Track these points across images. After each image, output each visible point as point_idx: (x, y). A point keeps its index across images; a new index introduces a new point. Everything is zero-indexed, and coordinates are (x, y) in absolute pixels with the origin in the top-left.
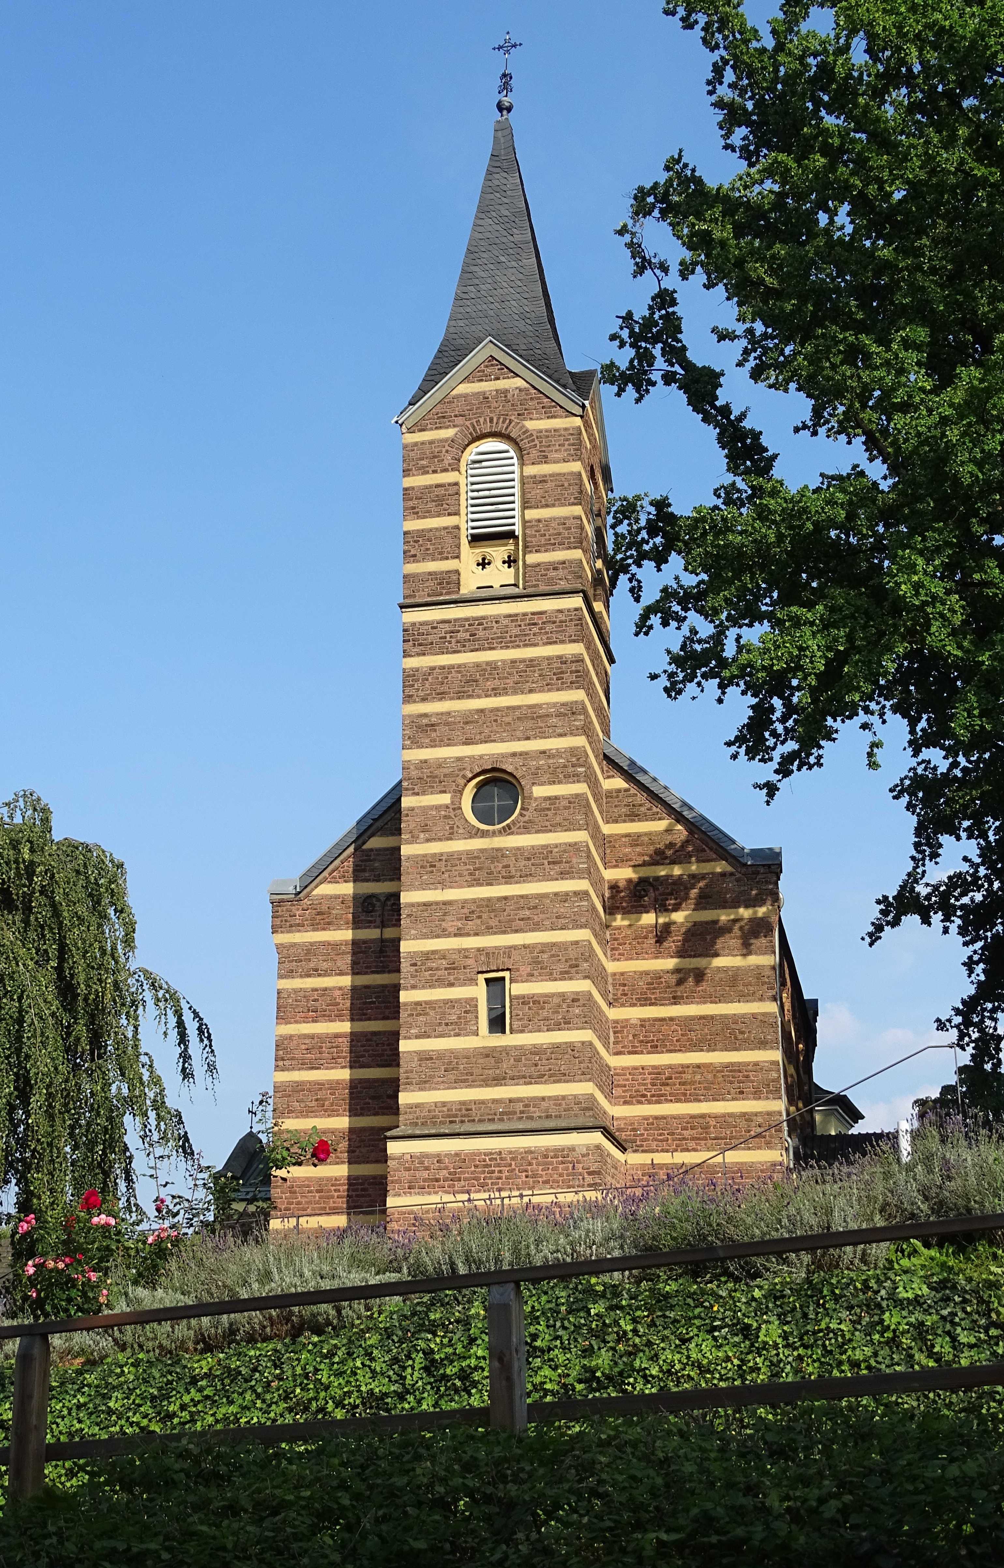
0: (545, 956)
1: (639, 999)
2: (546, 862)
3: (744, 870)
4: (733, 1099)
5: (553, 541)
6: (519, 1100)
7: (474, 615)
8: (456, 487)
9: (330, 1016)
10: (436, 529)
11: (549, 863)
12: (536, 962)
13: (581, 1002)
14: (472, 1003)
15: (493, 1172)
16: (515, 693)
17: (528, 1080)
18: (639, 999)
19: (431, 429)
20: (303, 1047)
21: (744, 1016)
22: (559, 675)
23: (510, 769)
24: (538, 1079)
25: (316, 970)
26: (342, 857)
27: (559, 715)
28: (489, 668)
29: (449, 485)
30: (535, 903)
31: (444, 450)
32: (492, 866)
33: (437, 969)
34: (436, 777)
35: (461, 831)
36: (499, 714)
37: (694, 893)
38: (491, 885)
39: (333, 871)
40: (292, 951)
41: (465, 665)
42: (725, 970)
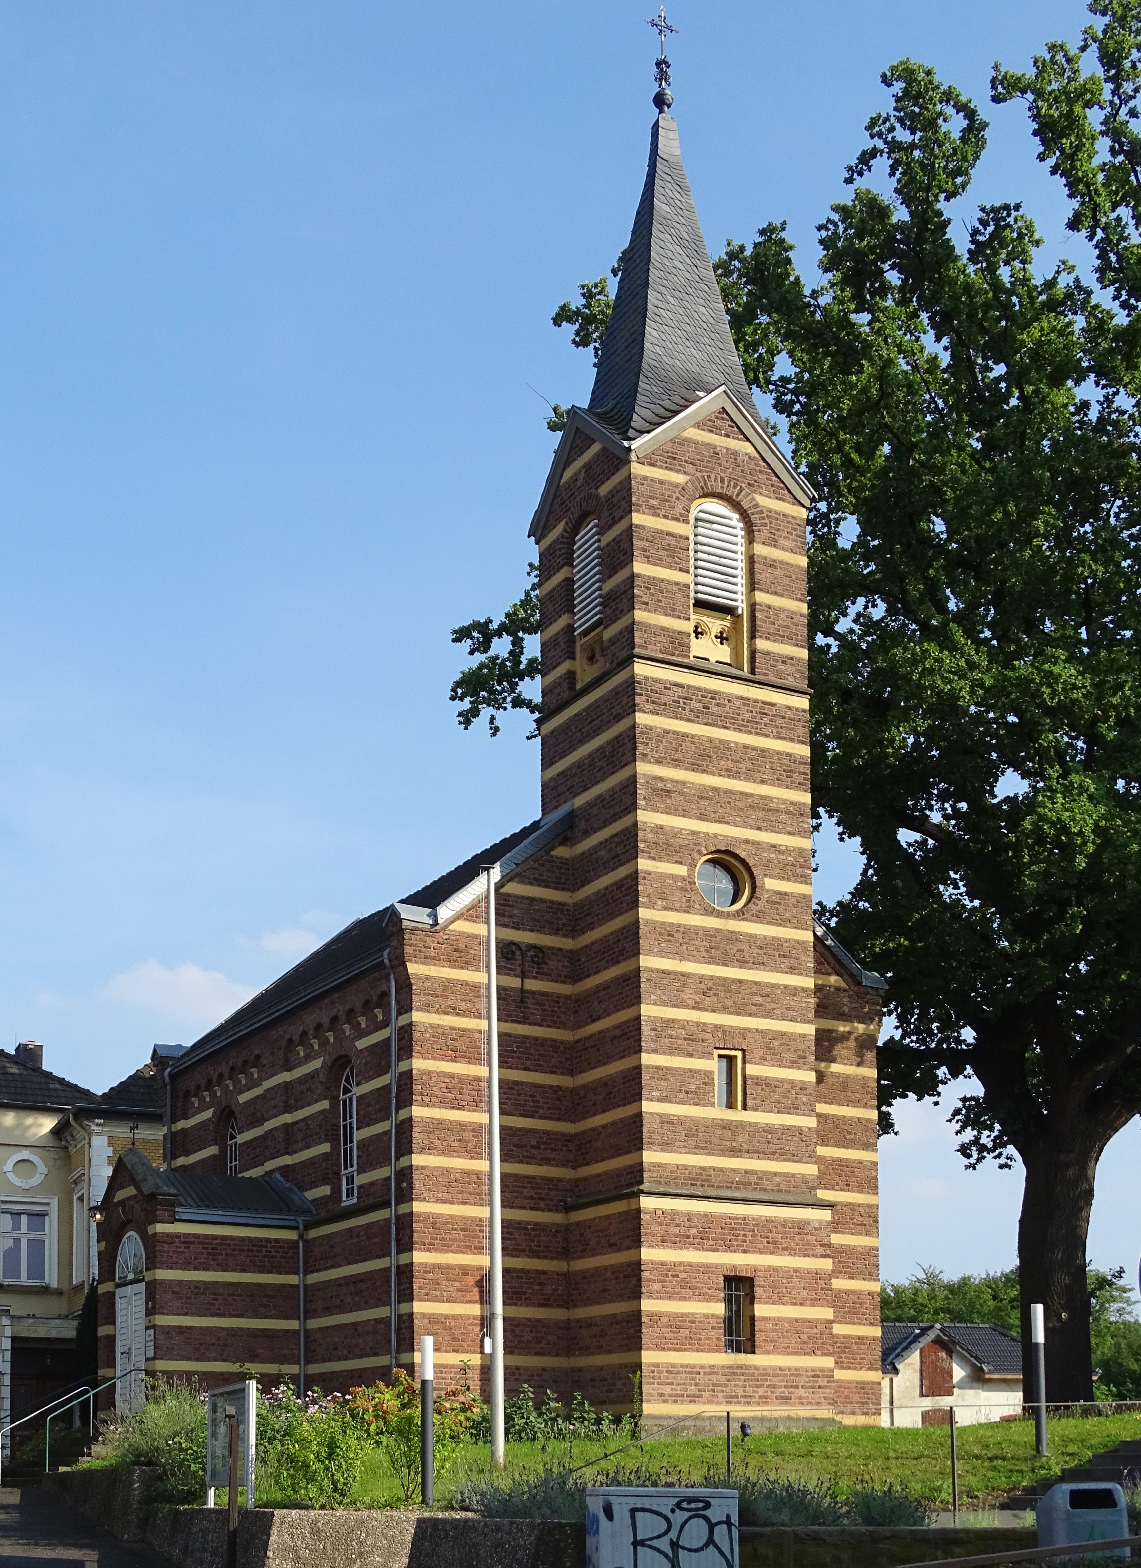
0: (776, 1043)
2: (777, 954)
3: (856, 989)
4: (841, 1190)
5: (781, 633)
6: (754, 1172)
9: (470, 1058)
12: (768, 1047)
14: (709, 1074)
15: (738, 1235)
16: (747, 779)
17: (761, 1156)
19: (661, 467)
20: (444, 1085)
21: (851, 1119)
23: (743, 855)
24: (771, 1155)
25: (454, 1009)
29: (681, 537)
30: (767, 991)
31: (675, 496)
32: (728, 947)
33: (676, 1038)
40: (428, 984)
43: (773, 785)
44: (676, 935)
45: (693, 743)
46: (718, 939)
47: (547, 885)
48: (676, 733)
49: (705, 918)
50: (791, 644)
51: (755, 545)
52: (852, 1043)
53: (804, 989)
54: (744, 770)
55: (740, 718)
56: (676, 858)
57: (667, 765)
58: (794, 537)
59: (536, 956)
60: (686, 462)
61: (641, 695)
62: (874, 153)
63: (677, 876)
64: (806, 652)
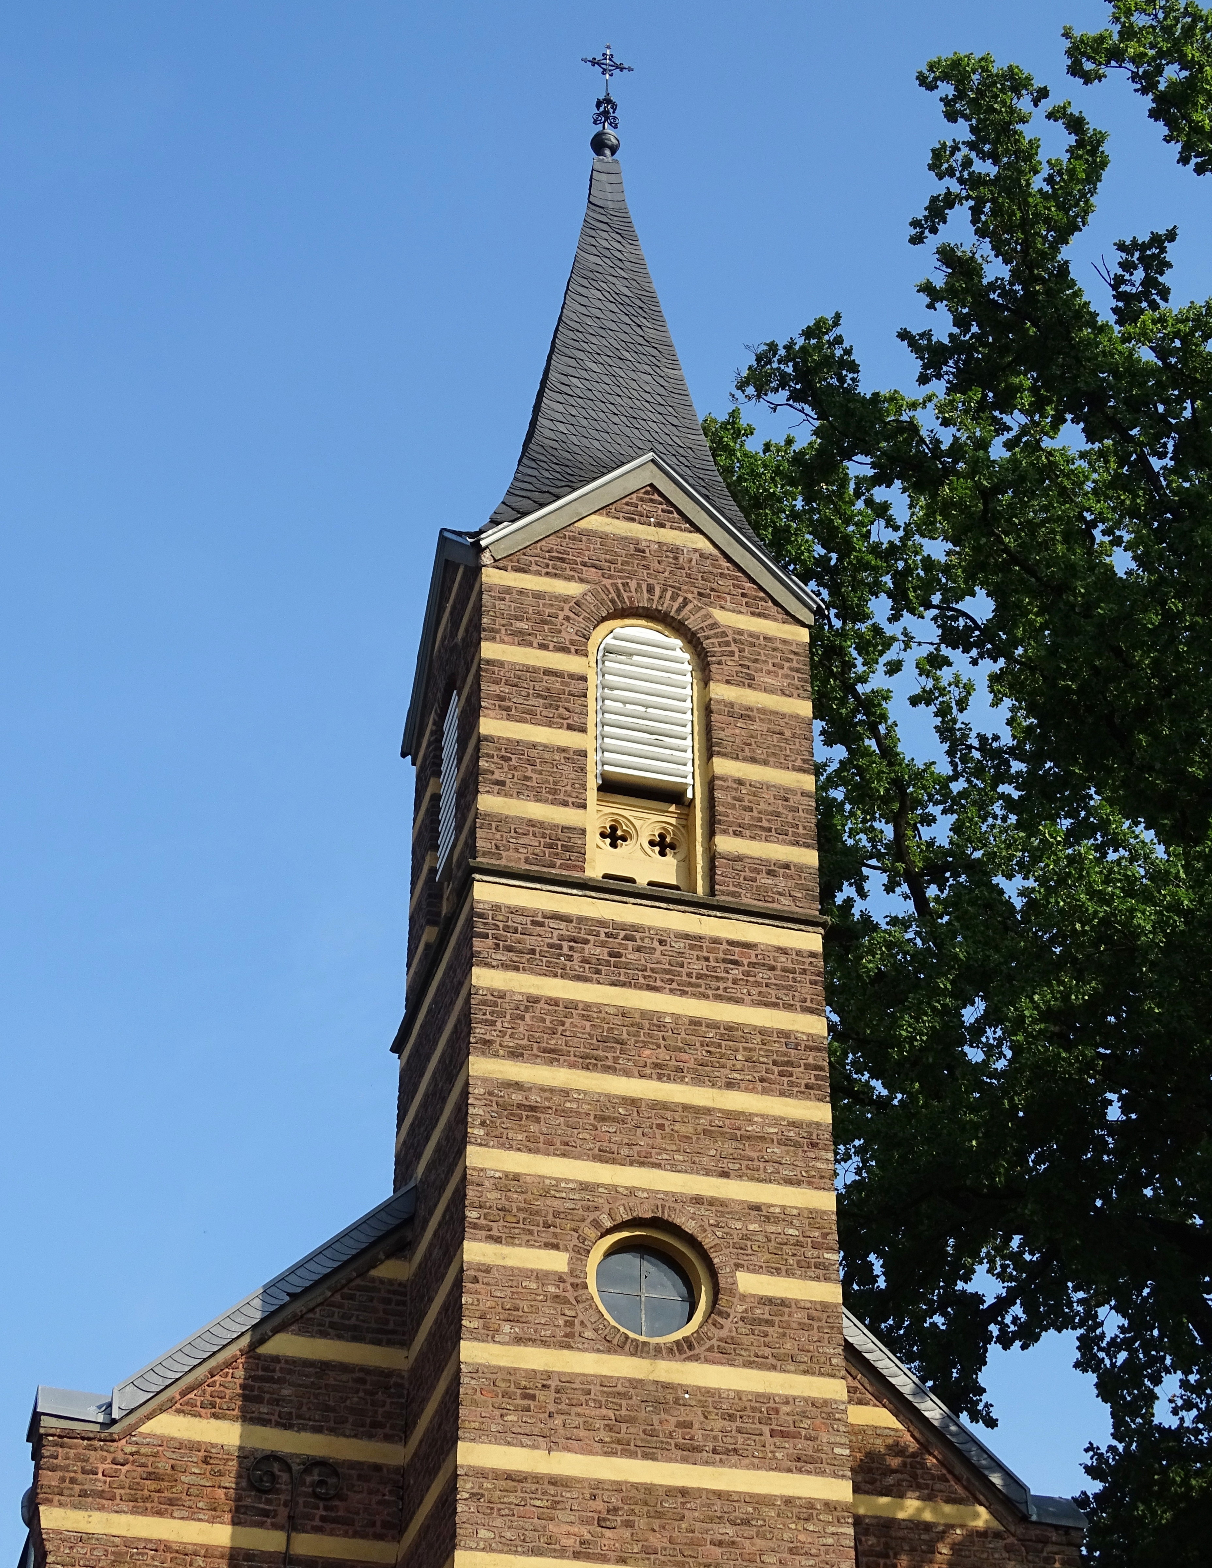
2: (766, 1429)
3: (1020, 1530)
5: (765, 824)
7: (618, 919)
8: (581, 685)
16: (698, 1080)
19: (539, 573)
23: (690, 1227)
26: (212, 1363)
28: (646, 1024)
29: (571, 676)
31: (561, 615)
32: (655, 1419)
34: (537, 1213)
36: (669, 1115)
38: (654, 1458)
39: (190, 1389)
40: (81, 1550)
43: (753, 1090)
44: (541, 1395)
45: (588, 1018)
46: (635, 1400)
47: (356, 1335)
48: (554, 1002)
49: (606, 1357)
50: (784, 842)
51: (712, 685)
53: (829, 1506)
54: (691, 1064)
55: (684, 971)
56: (546, 1237)
57: (534, 1059)
58: (786, 671)
59: (321, 1483)
60: (584, 564)
61: (486, 936)
62: (950, 200)
63: (547, 1274)
64: (815, 854)
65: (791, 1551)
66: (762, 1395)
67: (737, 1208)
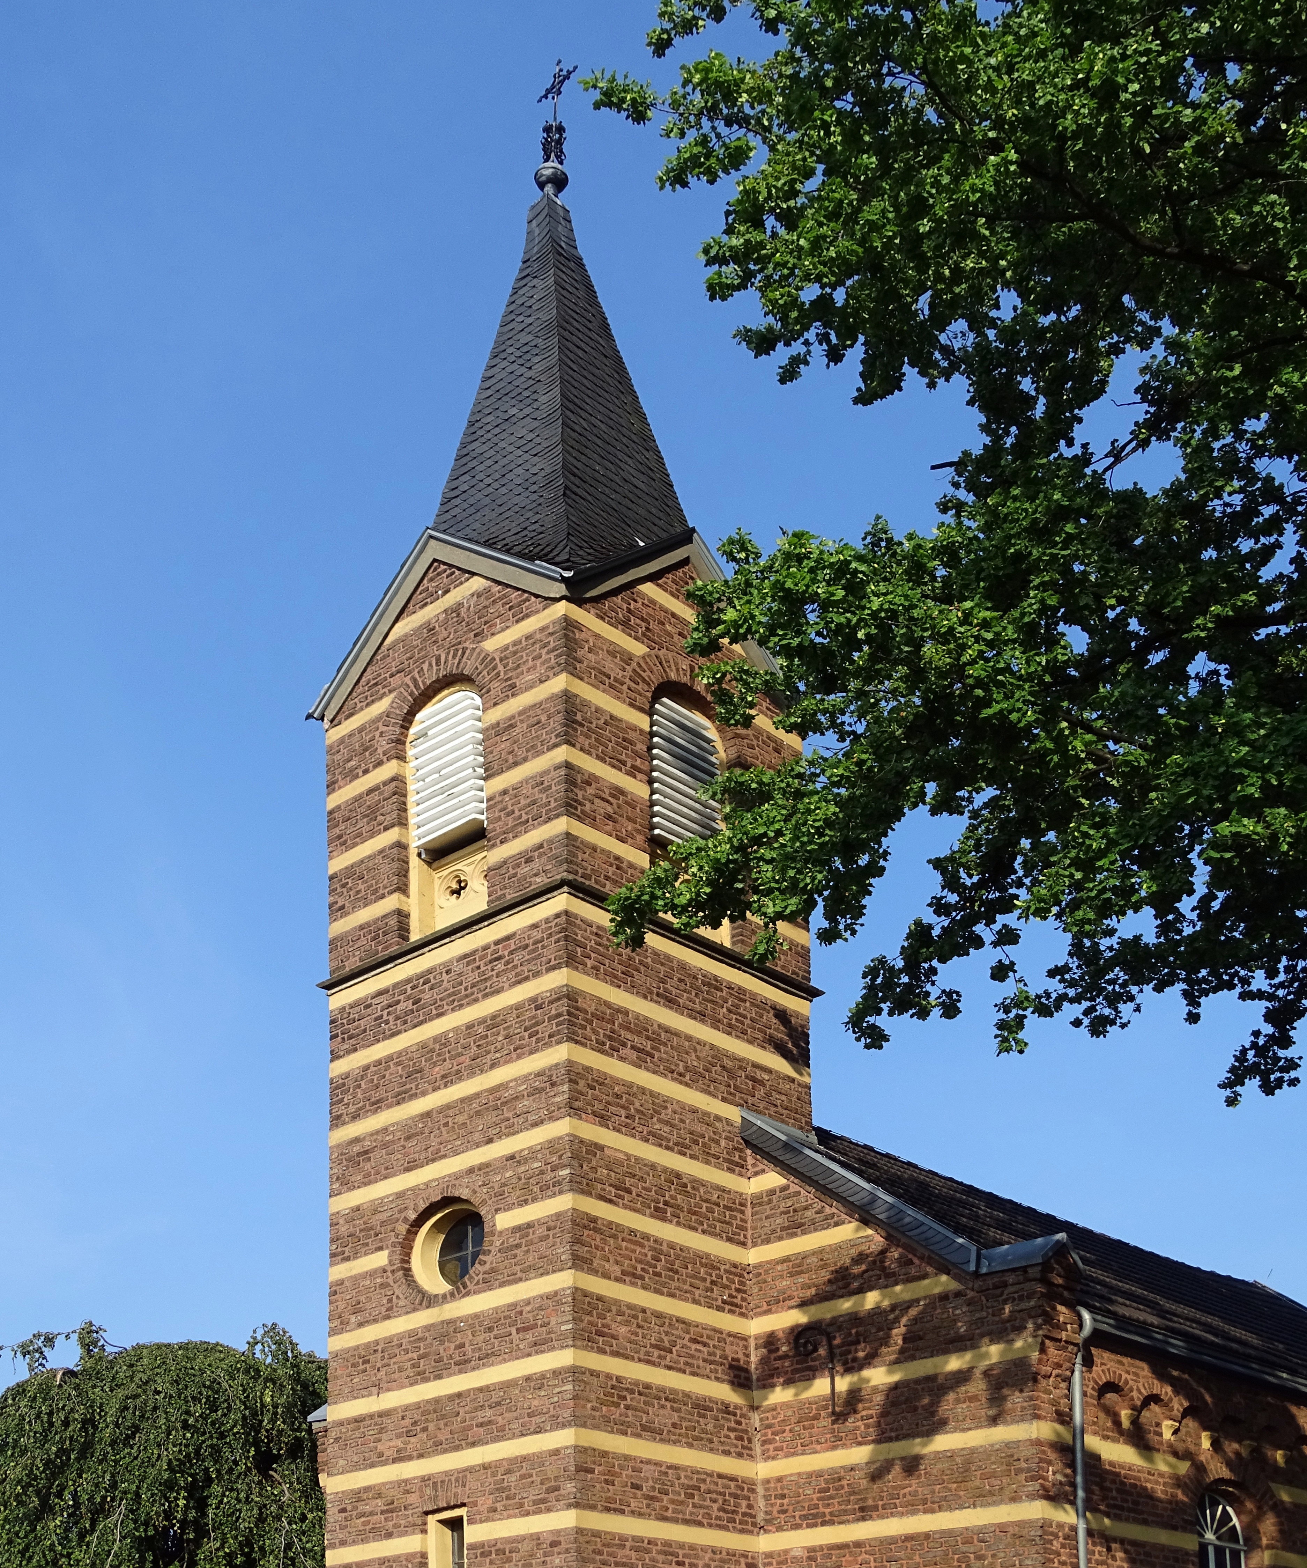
0: (513, 1478)
1: (804, 1517)
2: (513, 1330)
3: (979, 1283)
5: (524, 817)
10: (369, 857)
11: (518, 1331)
12: (500, 1489)
13: (564, 1546)
16: (472, 1074)
18: (804, 1517)
22: (532, 1030)
27: (535, 1092)
28: (437, 1047)
31: (377, 733)
33: (372, 1514)
35: (402, 1303)
36: (451, 1112)
37: (898, 1333)
41: (406, 1050)
42: (950, 1456)
45: (398, 1064)
52: (978, 1386)
65: (529, 1415)
66: (509, 1305)
67: (498, 1164)
